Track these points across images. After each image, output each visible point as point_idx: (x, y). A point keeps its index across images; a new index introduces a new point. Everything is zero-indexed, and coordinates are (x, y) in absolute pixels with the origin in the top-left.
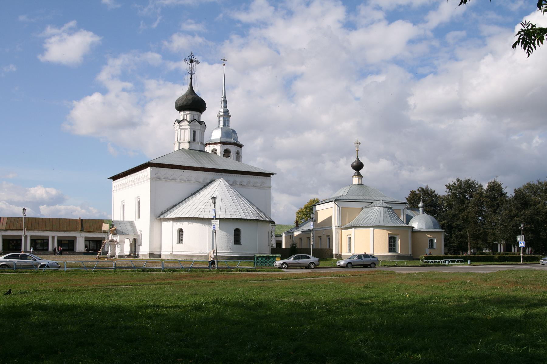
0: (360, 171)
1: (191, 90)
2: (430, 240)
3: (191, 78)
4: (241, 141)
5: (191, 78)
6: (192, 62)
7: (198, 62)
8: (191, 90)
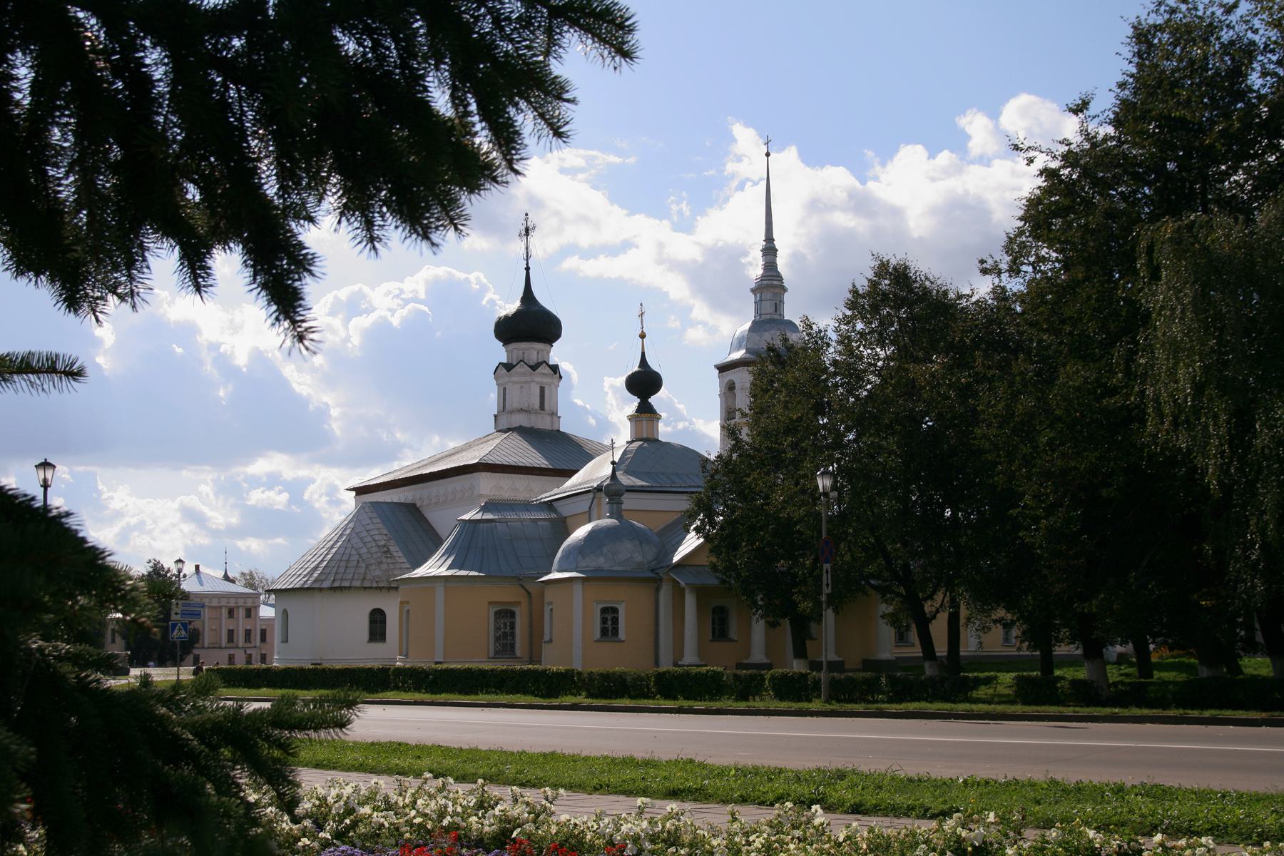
2: (604, 611)
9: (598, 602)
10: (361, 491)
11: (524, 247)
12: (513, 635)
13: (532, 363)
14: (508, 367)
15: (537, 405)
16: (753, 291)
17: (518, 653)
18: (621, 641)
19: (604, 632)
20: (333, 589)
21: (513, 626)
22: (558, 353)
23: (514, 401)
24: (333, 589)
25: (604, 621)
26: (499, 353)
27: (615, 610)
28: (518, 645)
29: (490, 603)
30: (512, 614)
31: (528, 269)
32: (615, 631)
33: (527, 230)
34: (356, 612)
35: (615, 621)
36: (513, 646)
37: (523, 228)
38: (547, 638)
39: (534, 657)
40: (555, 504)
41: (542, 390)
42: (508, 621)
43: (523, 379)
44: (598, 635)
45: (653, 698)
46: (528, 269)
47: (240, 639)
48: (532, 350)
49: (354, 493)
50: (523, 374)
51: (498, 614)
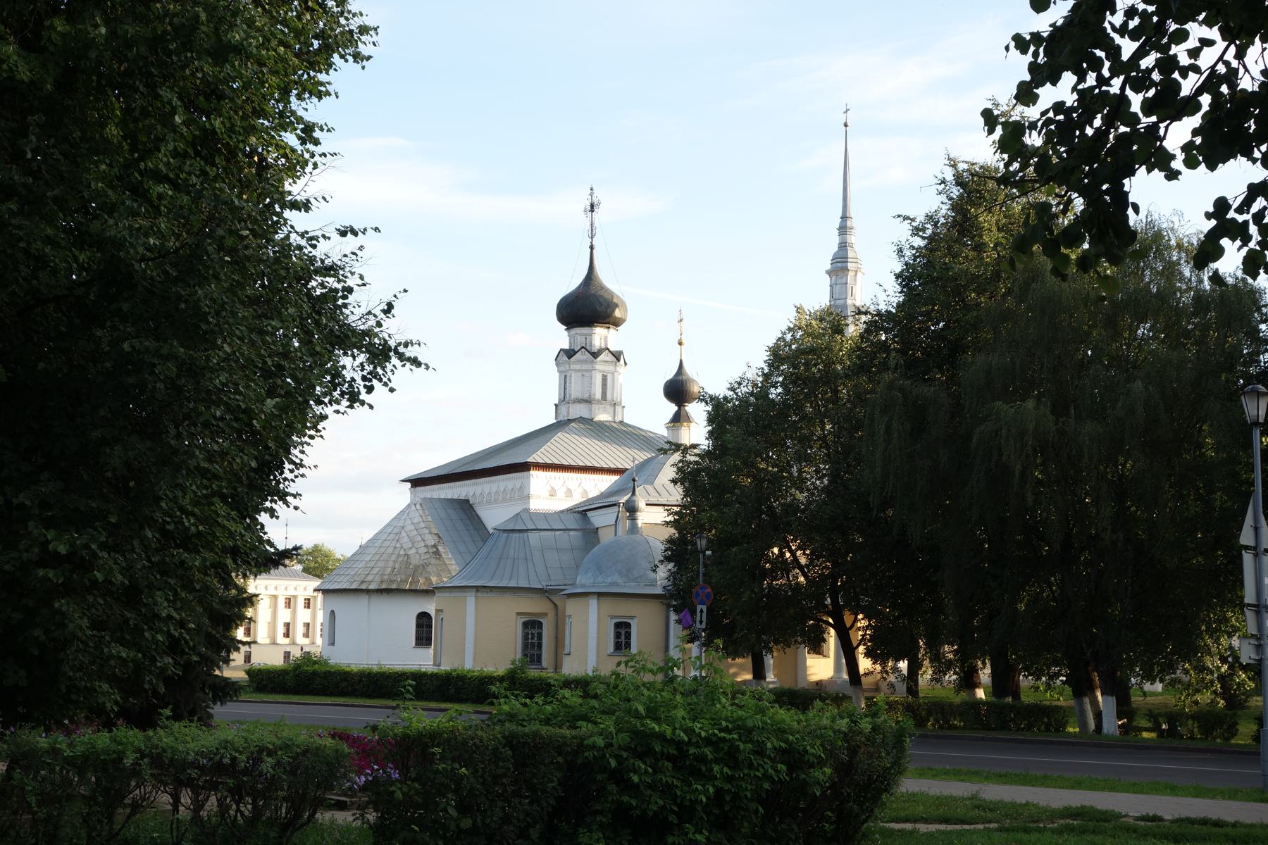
2: (618, 625)
10: (417, 482)
11: (588, 224)
12: (540, 646)
13: (595, 350)
14: (570, 353)
15: (598, 395)
16: (829, 272)
17: (544, 664)
19: (618, 646)
20: (380, 591)
21: (540, 636)
23: (575, 391)
24: (380, 591)
25: (618, 635)
26: (561, 337)
27: (628, 625)
28: (544, 656)
29: (518, 614)
30: (540, 624)
31: (592, 248)
32: (628, 645)
33: (592, 206)
34: (404, 615)
35: (628, 635)
36: (540, 656)
37: (588, 203)
38: (567, 651)
39: (557, 666)
40: (589, 514)
41: (604, 379)
42: (535, 631)
44: (611, 648)
45: (109, 725)
46: (592, 248)
47: (300, 630)
49: (409, 485)
50: (584, 362)
51: (525, 625)
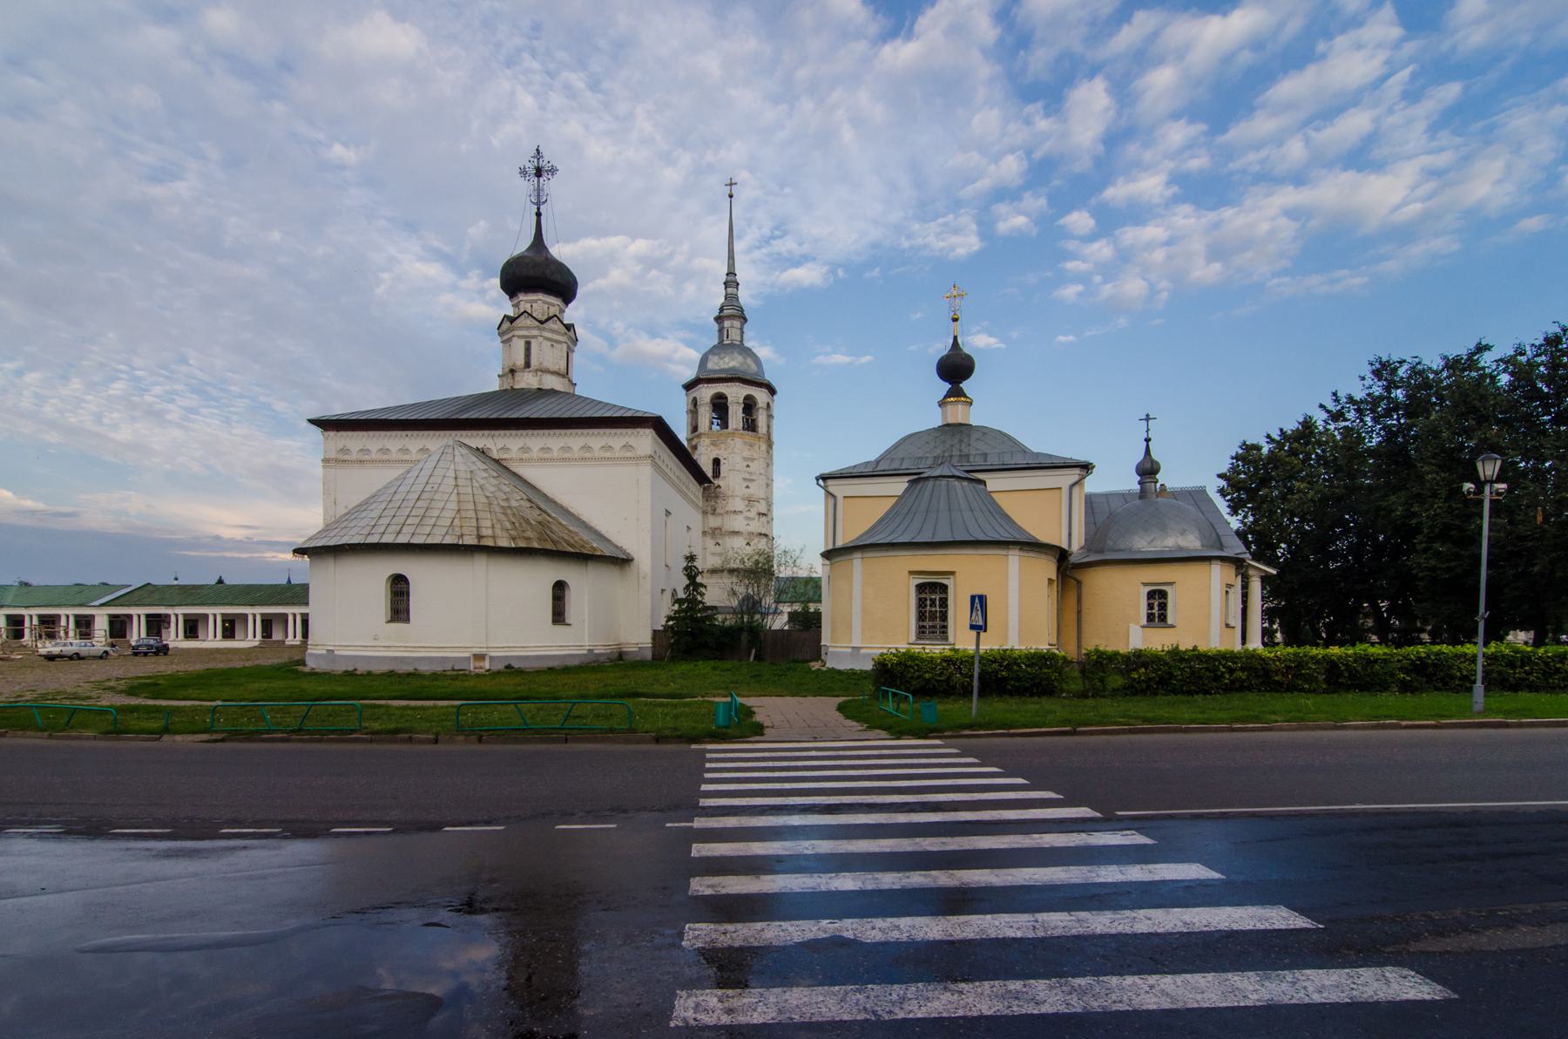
0: (964, 385)
1: (538, 241)
2: (1151, 595)
3: (539, 215)
4: (769, 377)
5: (539, 215)
6: (539, 172)
7: (553, 171)
8: (538, 241)
9: (1145, 584)
18: (1172, 626)
19: (1150, 618)
22: (572, 313)
25: (1150, 606)
32: (1163, 618)
35: (1163, 607)
43: (556, 337)
48: (540, 303)
